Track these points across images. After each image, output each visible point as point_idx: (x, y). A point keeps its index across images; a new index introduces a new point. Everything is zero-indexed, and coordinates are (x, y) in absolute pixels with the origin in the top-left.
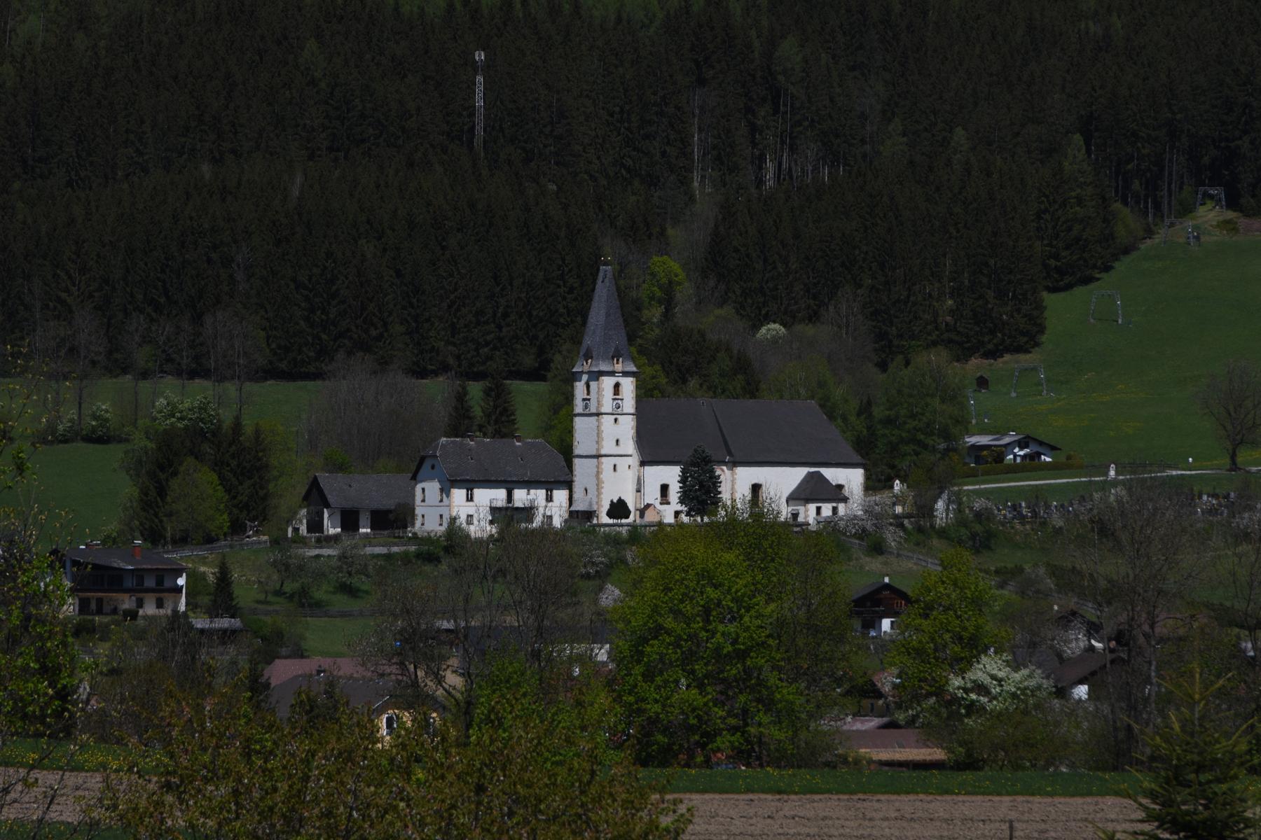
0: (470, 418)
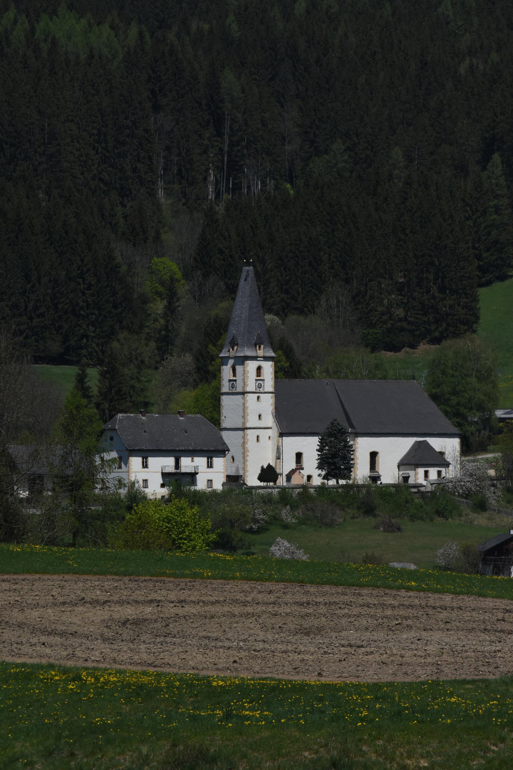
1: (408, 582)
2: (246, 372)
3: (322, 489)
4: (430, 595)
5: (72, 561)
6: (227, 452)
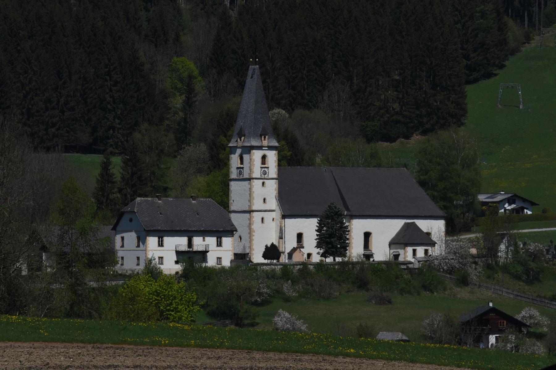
0: (113, 183)
1: (348, 349)
2: (252, 160)
3: (320, 266)
4: (364, 361)
5: (43, 330)
6: (235, 232)
